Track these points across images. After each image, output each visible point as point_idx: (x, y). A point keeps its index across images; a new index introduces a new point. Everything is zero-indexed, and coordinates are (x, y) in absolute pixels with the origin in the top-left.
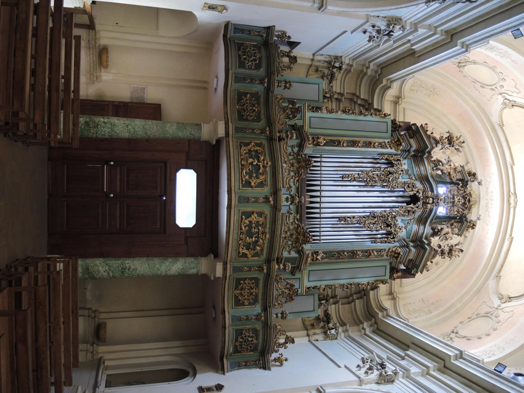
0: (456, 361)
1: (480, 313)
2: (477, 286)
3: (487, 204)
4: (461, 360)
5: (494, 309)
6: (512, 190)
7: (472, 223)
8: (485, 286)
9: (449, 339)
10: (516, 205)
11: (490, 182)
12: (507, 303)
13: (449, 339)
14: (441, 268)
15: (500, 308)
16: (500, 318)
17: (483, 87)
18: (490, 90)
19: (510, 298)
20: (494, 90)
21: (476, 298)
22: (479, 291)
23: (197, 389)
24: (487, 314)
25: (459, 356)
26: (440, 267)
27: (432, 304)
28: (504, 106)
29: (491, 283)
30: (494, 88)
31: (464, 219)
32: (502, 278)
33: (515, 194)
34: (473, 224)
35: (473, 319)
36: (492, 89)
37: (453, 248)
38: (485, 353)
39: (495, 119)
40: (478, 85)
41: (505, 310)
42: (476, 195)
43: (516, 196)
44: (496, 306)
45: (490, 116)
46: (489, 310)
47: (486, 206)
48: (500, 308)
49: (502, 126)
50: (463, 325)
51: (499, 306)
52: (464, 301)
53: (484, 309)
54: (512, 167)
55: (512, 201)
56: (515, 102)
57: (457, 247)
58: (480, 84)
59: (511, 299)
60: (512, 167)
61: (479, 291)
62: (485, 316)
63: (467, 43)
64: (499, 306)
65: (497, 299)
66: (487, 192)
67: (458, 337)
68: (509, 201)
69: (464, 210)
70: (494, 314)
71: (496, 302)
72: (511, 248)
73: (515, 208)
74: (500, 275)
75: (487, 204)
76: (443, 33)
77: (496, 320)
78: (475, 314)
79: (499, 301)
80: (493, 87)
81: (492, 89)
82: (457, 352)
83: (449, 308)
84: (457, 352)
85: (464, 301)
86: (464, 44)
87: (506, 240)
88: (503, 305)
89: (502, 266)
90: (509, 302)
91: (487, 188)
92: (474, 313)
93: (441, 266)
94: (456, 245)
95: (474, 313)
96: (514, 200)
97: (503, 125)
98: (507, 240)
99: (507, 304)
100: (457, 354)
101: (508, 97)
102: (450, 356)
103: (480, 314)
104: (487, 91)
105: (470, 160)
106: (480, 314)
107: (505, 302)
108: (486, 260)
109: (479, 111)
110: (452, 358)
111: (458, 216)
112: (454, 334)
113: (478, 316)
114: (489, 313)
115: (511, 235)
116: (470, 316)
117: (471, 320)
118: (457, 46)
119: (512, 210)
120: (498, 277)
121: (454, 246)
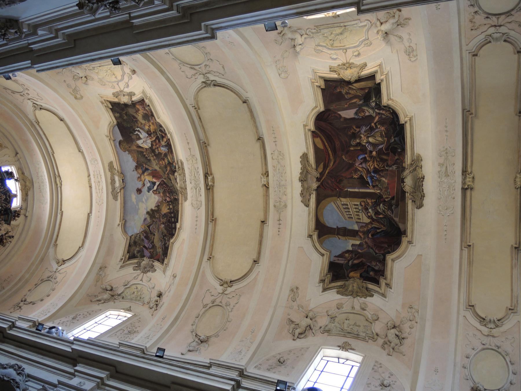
0: (11, 331)
1: (44, 278)
2: (40, 257)
3: (39, 186)
4: (14, 329)
5: (53, 272)
6: (57, 174)
7: (17, 213)
8: (47, 254)
9: (18, 308)
10: (62, 185)
11: (39, 168)
12: (62, 265)
13: (18, 308)
14: (8, 247)
15: (58, 271)
16: (58, 280)
17: (14, 93)
18: (20, 96)
19: (64, 261)
20: (23, 96)
21: (41, 265)
22: (42, 260)
23: (218, 38)
24: (49, 278)
25: (12, 326)
26: (7, 248)
27: (5, 281)
28: (35, 109)
29: (51, 250)
30: (22, 95)
31: (9, 211)
32: (58, 245)
33: (59, 176)
34: (18, 214)
35: (39, 285)
36: (21, 95)
37: (3, 237)
38: (43, 313)
39: (32, 117)
40: (10, 92)
41: (61, 272)
42: (30, 180)
43: (60, 178)
44: (54, 270)
45: (27, 115)
46: (50, 274)
47: (39, 188)
48: (58, 271)
49: (38, 123)
50: (30, 292)
51: (57, 269)
52: (31, 271)
53: (48, 274)
54: (53, 155)
55: (58, 182)
56: (41, 106)
57: (7, 235)
58: (11, 91)
59: (65, 262)
60: (53, 155)
61: (42, 260)
62: (47, 280)
63: (214, 27)
64: (57, 269)
65: (56, 263)
66: (38, 176)
67: (26, 304)
68: (56, 182)
69: (7, 205)
70: (53, 277)
71: (55, 266)
72: (62, 220)
73: (61, 188)
74: (57, 243)
75: (39, 186)
76: (180, 10)
77: (55, 282)
78: (40, 280)
79: (57, 265)
80: (22, 94)
81: (21, 95)
82: (10, 324)
83: (20, 280)
84: (10, 324)
85: (31, 271)
86: (209, 27)
87: (58, 214)
88: (60, 268)
89: (58, 236)
90: (64, 264)
91: (37, 173)
92: (39, 279)
93: (8, 247)
94: (5, 234)
95: (39, 279)
96: (60, 182)
97: (39, 122)
98: (59, 214)
99: (63, 266)
100: (10, 325)
101: (35, 102)
102: (5, 328)
103: (43, 279)
104: (17, 96)
105: (19, 151)
106: (43, 279)
107: (61, 266)
108: (44, 234)
109: (16, 110)
110: (7, 329)
111: (2, 210)
112: (23, 303)
113: (43, 281)
114: (50, 277)
115: (61, 210)
116: (36, 283)
117: (37, 286)
118: (201, 30)
119: (59, 189)
120: (56, 245)
121: (4, 235)
